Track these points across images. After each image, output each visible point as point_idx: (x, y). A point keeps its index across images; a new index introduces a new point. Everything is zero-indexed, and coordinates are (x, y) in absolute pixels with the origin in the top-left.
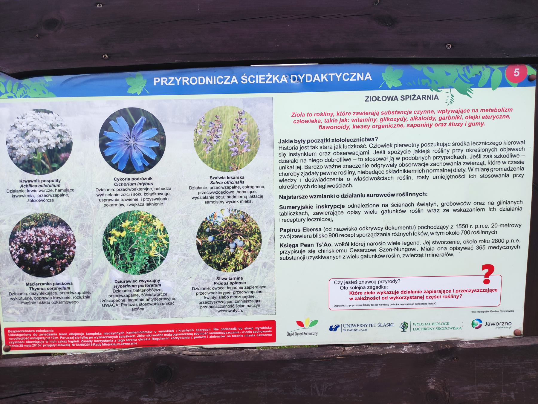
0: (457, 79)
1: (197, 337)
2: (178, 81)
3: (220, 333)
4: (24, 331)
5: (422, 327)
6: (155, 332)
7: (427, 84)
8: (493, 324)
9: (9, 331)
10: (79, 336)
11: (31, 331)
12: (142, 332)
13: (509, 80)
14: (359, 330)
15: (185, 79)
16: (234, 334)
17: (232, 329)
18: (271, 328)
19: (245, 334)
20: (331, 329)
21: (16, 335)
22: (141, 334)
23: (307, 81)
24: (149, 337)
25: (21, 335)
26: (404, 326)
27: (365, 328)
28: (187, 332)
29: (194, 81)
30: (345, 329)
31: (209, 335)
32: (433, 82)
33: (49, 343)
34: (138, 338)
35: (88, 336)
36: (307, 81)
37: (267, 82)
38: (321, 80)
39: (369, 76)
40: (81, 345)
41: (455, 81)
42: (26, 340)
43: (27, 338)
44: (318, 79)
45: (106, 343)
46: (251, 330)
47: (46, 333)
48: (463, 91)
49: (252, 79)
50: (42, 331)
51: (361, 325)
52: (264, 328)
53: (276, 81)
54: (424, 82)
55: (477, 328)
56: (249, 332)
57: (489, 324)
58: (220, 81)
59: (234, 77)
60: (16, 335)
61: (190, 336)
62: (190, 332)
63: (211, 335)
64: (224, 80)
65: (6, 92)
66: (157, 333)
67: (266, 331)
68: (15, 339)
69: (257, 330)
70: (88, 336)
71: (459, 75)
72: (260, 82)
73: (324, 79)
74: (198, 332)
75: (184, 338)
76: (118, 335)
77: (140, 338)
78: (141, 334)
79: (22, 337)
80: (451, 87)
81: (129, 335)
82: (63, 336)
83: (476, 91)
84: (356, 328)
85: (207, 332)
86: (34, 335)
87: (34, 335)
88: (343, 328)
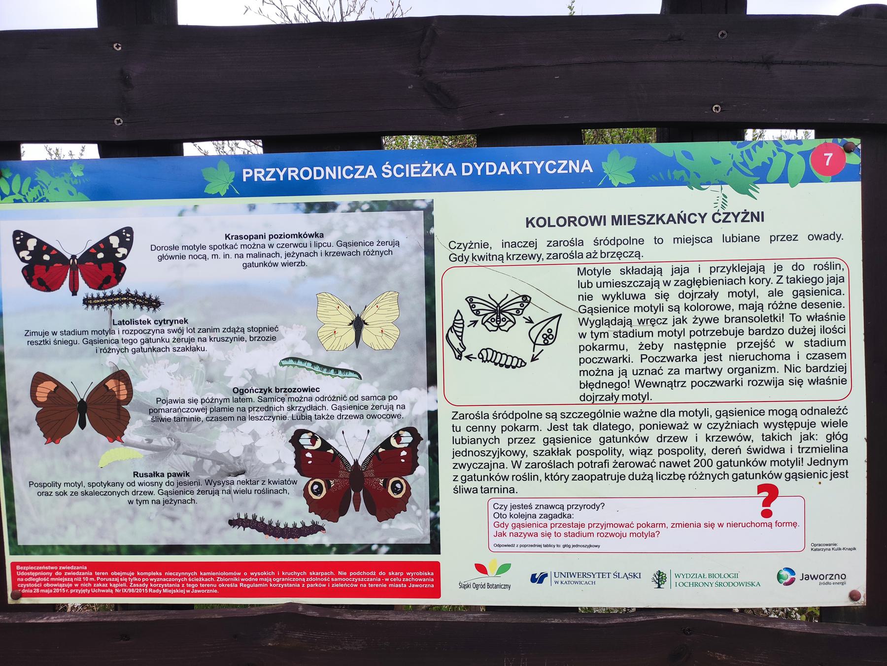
0: (731, 169)
1: (312, 585)
2: (281, 174)
3: (349, 580)
5: (692, 580)
7: (682, 177)
8: (814, 577)
10: (127, 577)
11: (52, 568)
12: (224, 574)
13: (817, 170)
14: (581, 583)
15: (293, 171)
16: (371, 583)
17: (368, 574)
18: (432, 574)
19: (390, 582)
20: (533, 579)
21: (28, 574)
22: (222, 577)
23: (488, 173)
24: (235, 582)
25: (36, 574)
27: (592, 579)
28: (295, 577)
29: (306, 174)
30: (557, 579)
32: (692, 175)
33: (79, 588)
35: (141, 577)
36: (488, 173)
37: (424, 174)
40: (130, 591)
41: (728, 174)
42: (43, 583)
43: (45, 579)
44: (506, 170)
47: (76, 571)
50: (69, 568)
51: (584, 576)
52: (420, 573)
53: (437, 172)
54: (677, 174)
57: (807, 577)
60: (28, 574)
61: (300, 583)
62: (300, 576)
63: (334, 582)
65: (12, 193)
66: (249, 576)
69: (409, 577)
71: (734, 164)
72: (413, 175)
74: (314, 576)
76: (187, 577)
77: (221, 583)
78: (222, 577)
79: (38, 577)
80: (722, 183)
81: (205, 577)
84: (576, 579)
85: (327, 576)
86: (57, 573)
87: (57, 573)
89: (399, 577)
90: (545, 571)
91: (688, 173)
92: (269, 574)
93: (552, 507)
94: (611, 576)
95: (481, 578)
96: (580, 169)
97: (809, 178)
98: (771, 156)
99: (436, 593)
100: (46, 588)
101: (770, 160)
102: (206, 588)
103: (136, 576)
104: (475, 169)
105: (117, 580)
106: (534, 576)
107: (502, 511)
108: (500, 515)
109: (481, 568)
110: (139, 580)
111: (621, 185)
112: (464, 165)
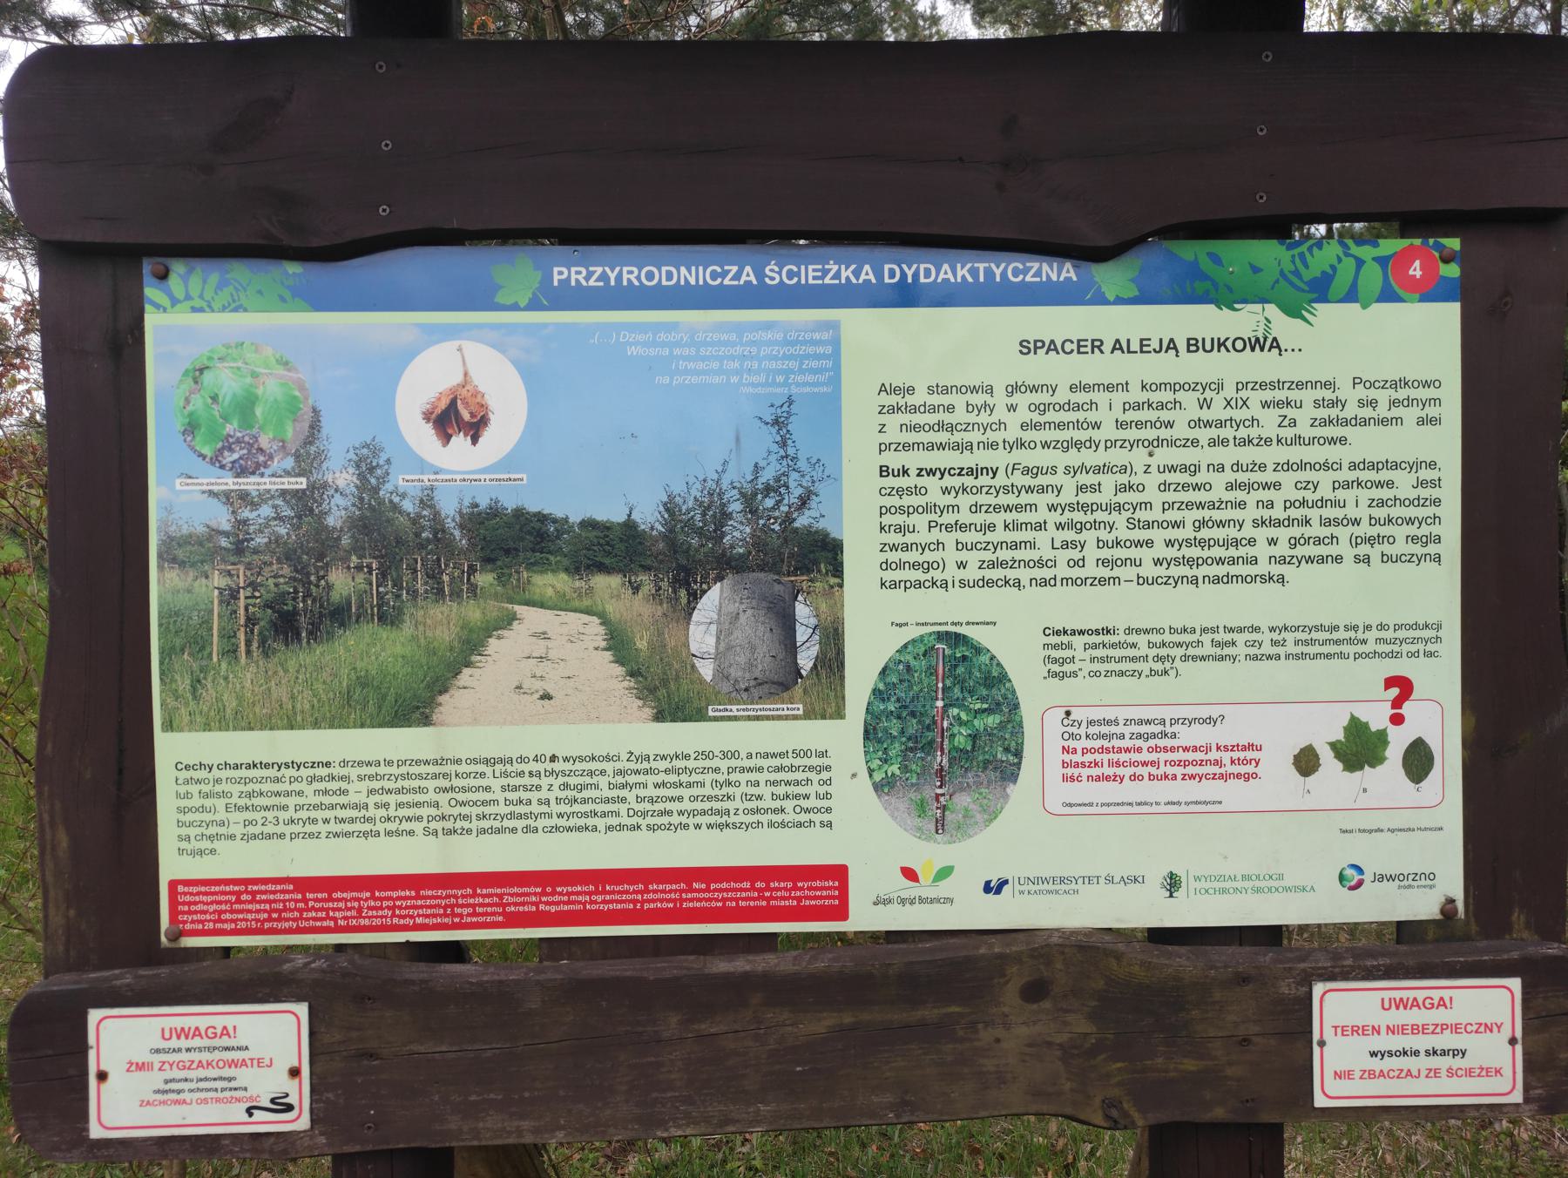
0: (1277, 281)
1: (652, 906)
2: (612, 276)
4: (217, 889)
6: (549, 889)
8: (1391, 878)
9: (180, 888)
10: (358, 900)
12: (516, 890)
15: (631, 272)
19: (772, 898)
20: (987, 888)
22: (512, 895)
24: (533, 904)
25: (210, 898)
26: (1173, 884)
28: (627, 892)
33: (279, 920)
34: (504, 906)
36: (922, 280)
37: (827, 281)
38: (955, 276)
40: (363, 922)
42: (220, 912)
43: (223, 907)
44: (950, 276)
46: (785, 889)
47: (274, 892)
48: (1293, 311)
49: (790, 275)
50: (263, 888)
51: (1062, 881)
53: (848, 278)
54: (1200, 287)
55: (1352, 888)
57: (1381, 878)
61: (635, 902)
62: (635, 892)
64: (724, 274)
65: (188, 297)
66: (554, 893)
68: (193, 908)
69: (802, 889)
71: (1282, 273)
72: (811, 281)
73: (963, 277)
74: (655, 892)
75: (619, 906)
76: (456, 897)
77: (510, 904)
78: (512, 895)
80: (1264, 301)
81: (484, 896)
82: (316, 900)
83: (1327, 314)
84: (1051, 887)
86: (244, 897)
87: (244, 897)
88: (1018, 887)
90: (1005, 876)
91: (1215, 285)
92: (585, 889)
93: (1148, 722)
94: (1102, 880)
97: (1388, 296)
98: (1335, 262)
99: (841, 913)
100: (226, 921)
101: (1333, 267)
103: (373, 898)
105: (341, 905)
106: (988, 883)
108: (1072, 736)
110: (378, 904)
112: (887, 267)
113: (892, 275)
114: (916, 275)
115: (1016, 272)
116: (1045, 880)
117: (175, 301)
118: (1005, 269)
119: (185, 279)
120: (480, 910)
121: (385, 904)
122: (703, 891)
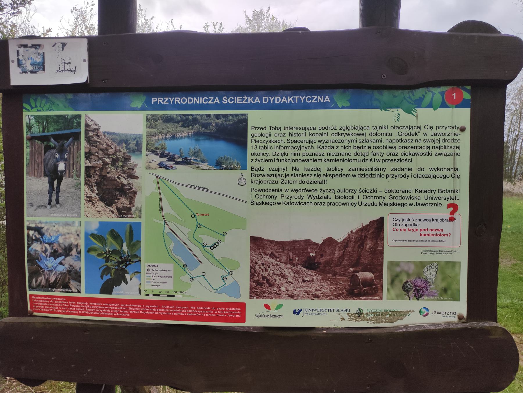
1: (177, 314)
2: (172, 101)
3: (196, 311)
8: (439, 313)
9: (33, 297)
10: (84, 305)
12: (133, 306)
15: (177, 99)
19: (217, 313)
22: (131, 307)
23: (276, 102)
24: (138, 311)
25: (42, 301)
27: (325, 312)
28: (169, 309)
29: (184, 101)
31: (187, 313)
33: (62, 310)
34: (129, 311)
35: (91, 305)
36: (276, 102)
37: (244, 102)
38: (287, 101)
39: (327, 99)
42: (45, 306)
43: (45, 304)
44: (286, 101)
45: (106, 312)
46: (222, 310)
47: (60, 301)
49: (231, 100)
52: (234, 309)
53: (250, 101)
55: (424, 316)
56: (221, 312)
57: (435, 313)
58: (205, 102)
59: (217, 98)
61: (171, 312)
62: (171, 309)
63: (188, 313)
64: (209, 100)
65: (36, 107)
66: (145, 308)
67: (235, 312)
69: (227, 311)
70: (91, 305)
72: (238, 102)
73: (290, 101)
74: (178, 309)
76: (114, 306)
77: (131, 310)
78: (131, 307)
79: (42, 302)
80: (397, 107)
81: (123, 307)
82: (72, 304)
85: (185, 309)
86: (51, 301)
87: (51, 301)
88: (305, 312)
89: (222, 310)
90: (301, 308)
92: (155, 307)
95: (267, 312)
96: (324, 100)
97: (443, 105)
100: (46, 309)
102: (123, 313)
103: (89, 305)
104: (270, 100)
105: (79, 306)
106: (295, 310)
107: (397, 222)
108: (397, 224)
109: (267, 307)
110: (90, 307)
111: (343, 108)
112: (264, 98)
113: (266, 100)
114: (274, 100)
115: (309, 99)
116: (315, 310)
117: (32, 108)
118: (305, 98)
119: (35, 100)
120: (121, 311)
121: (92, 307)
122: (194, 310)
